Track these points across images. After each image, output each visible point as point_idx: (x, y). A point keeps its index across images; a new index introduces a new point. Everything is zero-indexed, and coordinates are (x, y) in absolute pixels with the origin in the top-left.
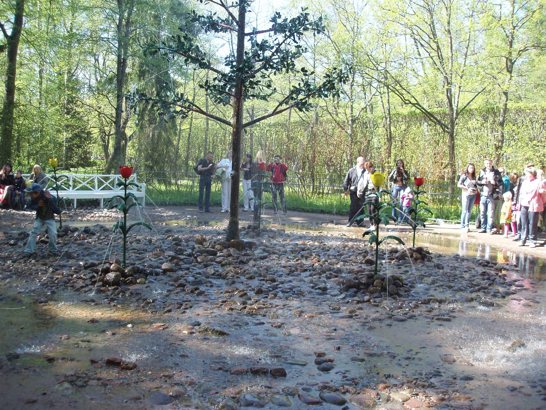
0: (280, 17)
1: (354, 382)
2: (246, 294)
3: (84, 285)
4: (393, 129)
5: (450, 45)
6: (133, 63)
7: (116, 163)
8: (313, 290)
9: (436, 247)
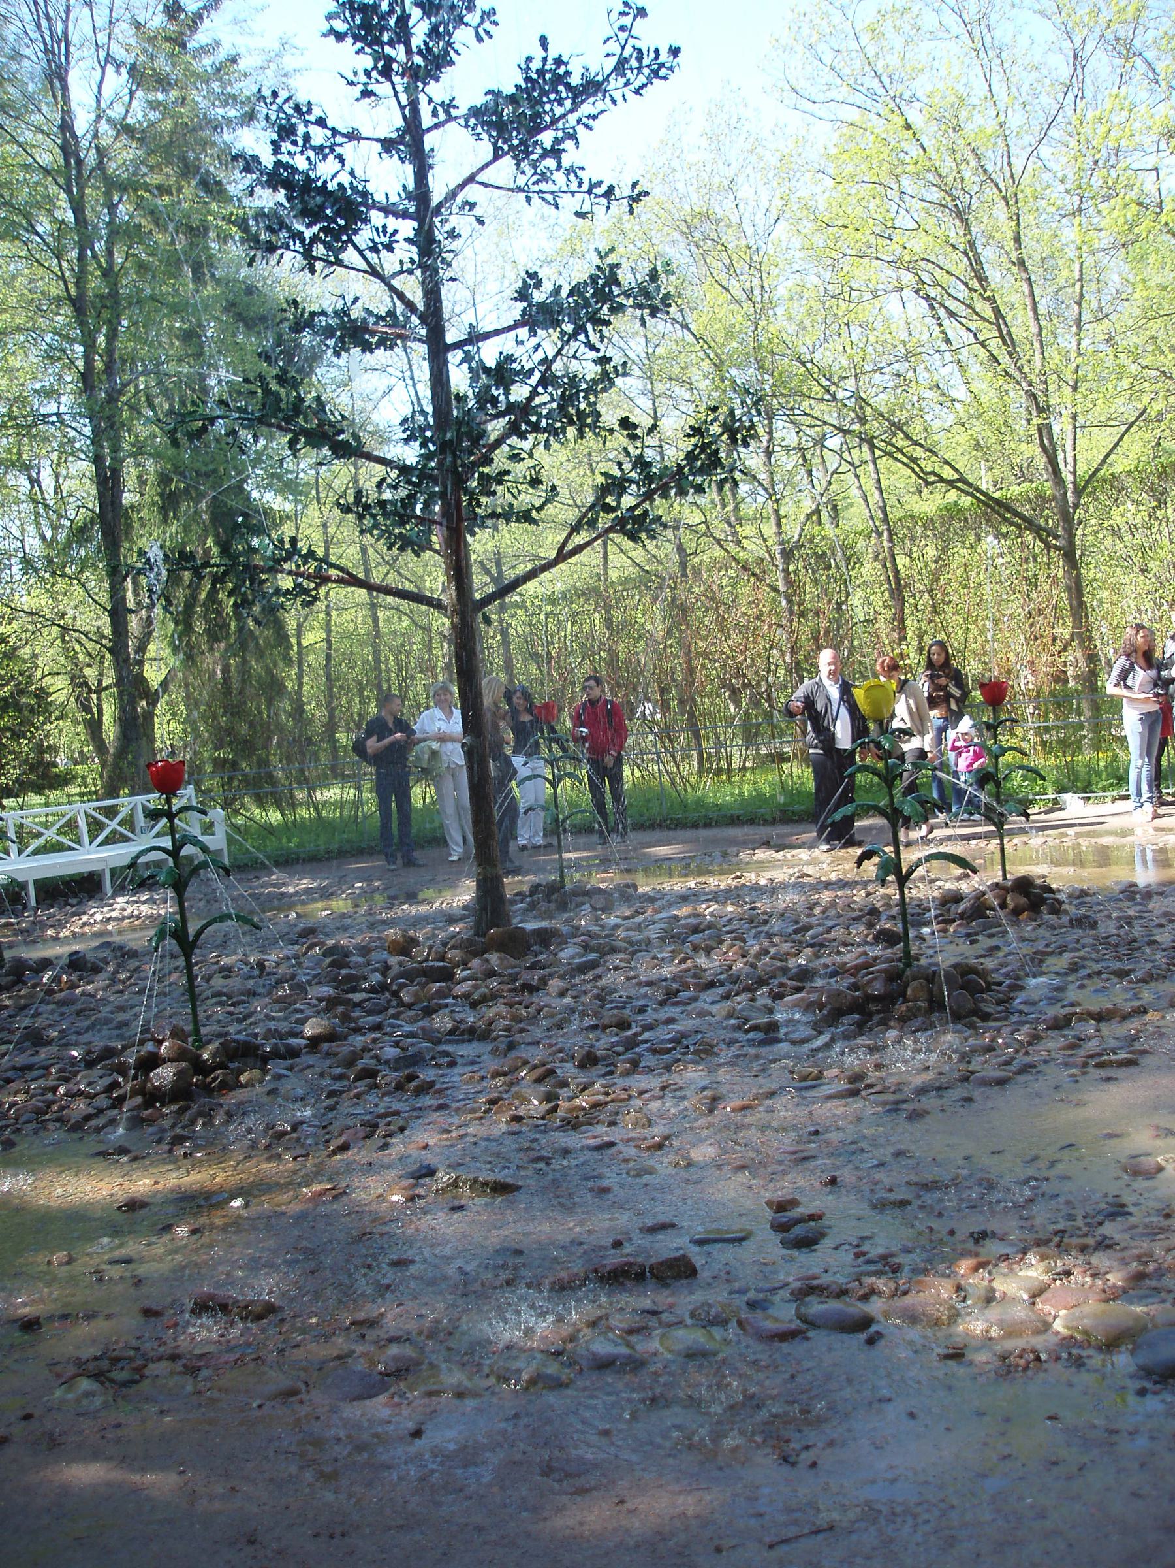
0: (539, 284)
1: (888, 1265)
2: (552, 1072)
3: (91, 1111)
4: (901, 561)
5: (1028, 301)
6: (139, 477)
7: (130, 764)
8: (739, 1035)
9: (1068, 871)
